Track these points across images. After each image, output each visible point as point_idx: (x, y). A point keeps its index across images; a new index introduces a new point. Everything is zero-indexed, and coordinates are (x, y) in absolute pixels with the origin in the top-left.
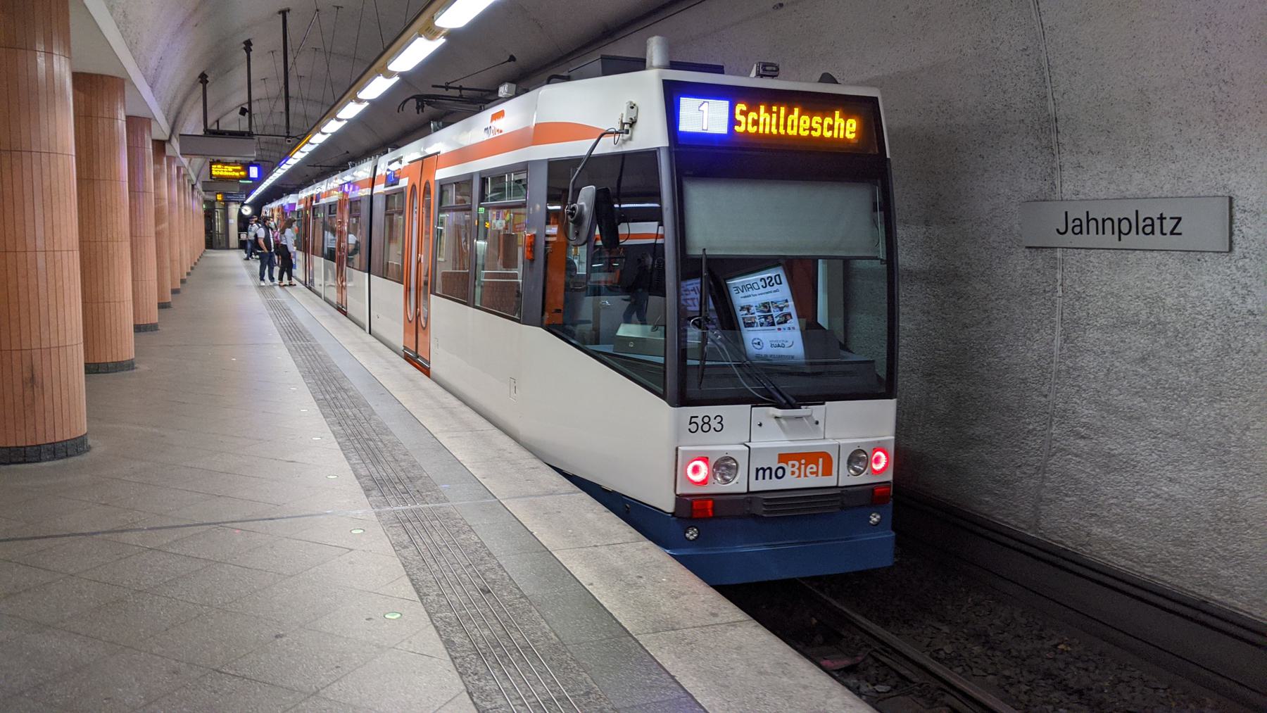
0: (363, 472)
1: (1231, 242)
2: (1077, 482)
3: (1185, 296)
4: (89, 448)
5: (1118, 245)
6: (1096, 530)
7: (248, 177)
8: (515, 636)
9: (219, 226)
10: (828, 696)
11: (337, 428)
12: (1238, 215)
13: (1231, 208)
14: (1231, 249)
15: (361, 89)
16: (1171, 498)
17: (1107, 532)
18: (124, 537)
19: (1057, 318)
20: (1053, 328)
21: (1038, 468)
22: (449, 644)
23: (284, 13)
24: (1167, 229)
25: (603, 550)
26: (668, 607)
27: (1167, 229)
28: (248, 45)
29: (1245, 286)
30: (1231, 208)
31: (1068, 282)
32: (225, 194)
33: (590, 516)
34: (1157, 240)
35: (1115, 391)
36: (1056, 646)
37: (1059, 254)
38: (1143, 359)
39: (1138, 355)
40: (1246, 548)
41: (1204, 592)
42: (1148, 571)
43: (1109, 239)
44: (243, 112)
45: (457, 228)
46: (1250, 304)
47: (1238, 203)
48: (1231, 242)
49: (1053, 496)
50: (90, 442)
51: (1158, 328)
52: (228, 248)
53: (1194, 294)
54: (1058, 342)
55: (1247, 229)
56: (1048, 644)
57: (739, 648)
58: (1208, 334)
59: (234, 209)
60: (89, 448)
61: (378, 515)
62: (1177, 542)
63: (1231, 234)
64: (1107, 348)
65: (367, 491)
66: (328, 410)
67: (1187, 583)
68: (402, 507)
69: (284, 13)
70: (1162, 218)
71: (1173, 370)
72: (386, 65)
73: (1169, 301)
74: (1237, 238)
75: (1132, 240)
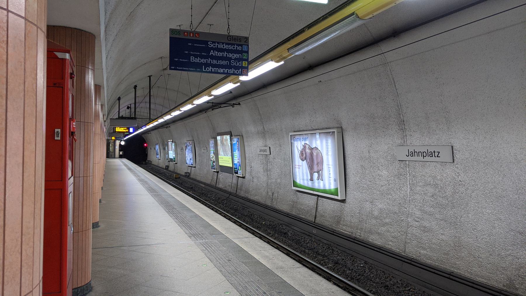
0: (188, 232)
1: (453, 159)
2: (416, 236)
3: (443, 176)
4: (99, 226)
5: (423, 160)
6: (422, 252)
7: (129, 131)
8: (238, 270)
9: (111, 149)
10: (321, 281)
11: (176, 220)
12: (455, 151)
13: (452, 149)
14: (453, 162)
15: (182, 107)
16: (442, 240)
17: (425, 252)
18: (122, 248)
19: (408, 183)
20: (407, 186)
21: (405, 232)
22: (221, 271)
23: (150, 77)
24: (436, 156)
25: (263, 251)
26: (281, 264)
27: (436, 156)
28: (135, 87)
29: (458, 173)
30: (452, 149)
31: (410, 172)
32: (116, 138)
33: (259, 243)
34: (433, 159)
35: (425, 206)
36: (410, 290)
37: (407, 162)
38: (433, 196)
39: (431, 195)
40: (463, 254)
41: (452, 269)
42: (437, 264)
43: (421, 158)
44: (128, 108)
45: (65, 59)
46: (460, 178)
47: (454, 148)
48: (453, 159)
49: (409, 241)
50: (100, 224)
51: (436, 186)
52: (115, 158)
53: (445, 175)
54: (409, 191)
55: (457, 156)
56: (407, 289)
57: (299, 272)
58: (450, 188)
59: (118, 142)
60: (99, 226)
61: (195, 243)
62: (445, 254)
63: (453, 157)
64: (422, 193)
65: (190, 237)
66: (171, 215)
67: (447, 267)
68: (201, 241)
69: (150, 77)
70: (434, 152)
71: (441, 199)
72: (193, 102)
73: (439, 178)
74: (455, 158)
75: (427, 158)
